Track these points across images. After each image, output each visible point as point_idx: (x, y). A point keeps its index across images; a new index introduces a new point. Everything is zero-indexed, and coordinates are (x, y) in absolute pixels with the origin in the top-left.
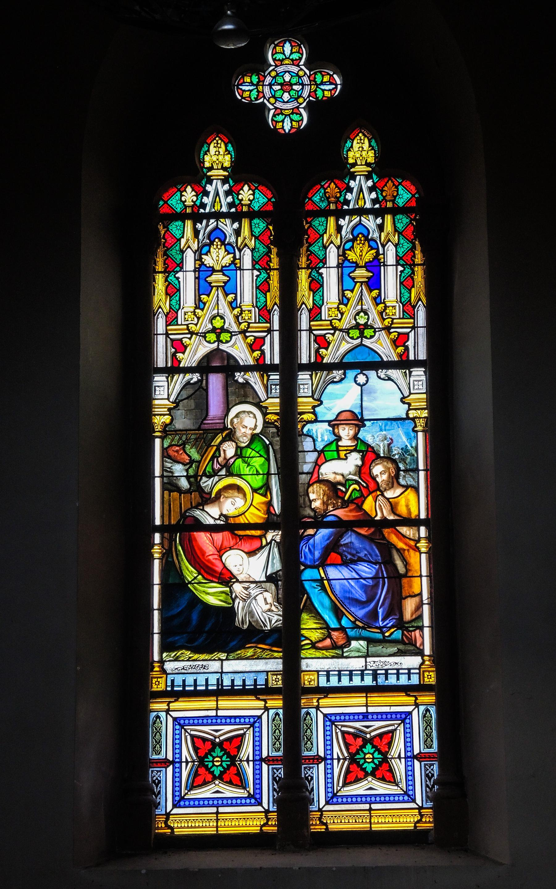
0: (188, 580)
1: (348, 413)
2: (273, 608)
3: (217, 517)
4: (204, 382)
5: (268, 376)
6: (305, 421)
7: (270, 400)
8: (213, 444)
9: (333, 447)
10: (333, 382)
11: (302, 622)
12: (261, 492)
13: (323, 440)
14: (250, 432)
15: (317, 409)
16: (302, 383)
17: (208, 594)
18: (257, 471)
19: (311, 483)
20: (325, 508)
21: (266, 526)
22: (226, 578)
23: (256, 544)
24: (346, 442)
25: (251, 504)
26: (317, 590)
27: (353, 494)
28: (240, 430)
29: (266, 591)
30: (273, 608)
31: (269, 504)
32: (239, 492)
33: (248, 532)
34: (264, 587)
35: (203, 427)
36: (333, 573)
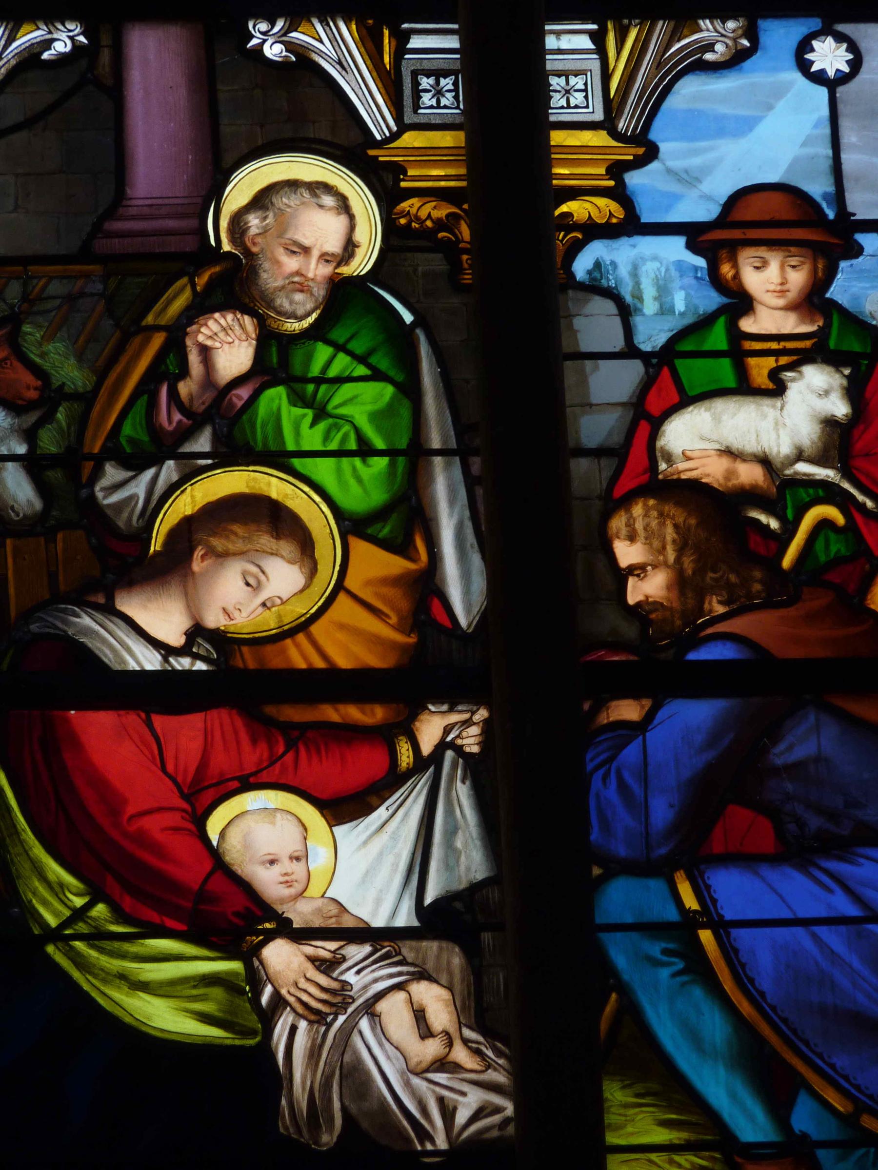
0: (43, 924)
1: (777, 198)
2: (460, 1054)
3: (176, 639)
4: (105, 57)
5: (402, 38)
6: (577, 227)
7: (410, 139)
8: (150, 319)
9: (717, 338)
10: (702, 67)
11: (611, 1118)
12: (385, 531)
13: (666, 310)
14: (326, 270)
15: (634, 179)
16: (559, 66)
17: (144, 987)
18: (361, 438)
19: (618, 493)
20: (691, 603)
21: (406, 686)
22: (234, 917)
23: (366, 763)
24: (770, 319)
25: (340, 587)
26: (664, 973)
27: (819, 545)
28: (277, 263)
29: (422, 975)
30: (460, 1054)
31: (426, 586)
32: (277, 534)
33: (331, 713)
34: (410, 956)
35: (102, 245)
36: (737, 890)
